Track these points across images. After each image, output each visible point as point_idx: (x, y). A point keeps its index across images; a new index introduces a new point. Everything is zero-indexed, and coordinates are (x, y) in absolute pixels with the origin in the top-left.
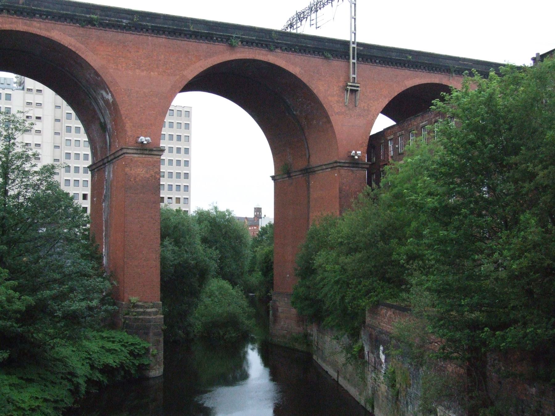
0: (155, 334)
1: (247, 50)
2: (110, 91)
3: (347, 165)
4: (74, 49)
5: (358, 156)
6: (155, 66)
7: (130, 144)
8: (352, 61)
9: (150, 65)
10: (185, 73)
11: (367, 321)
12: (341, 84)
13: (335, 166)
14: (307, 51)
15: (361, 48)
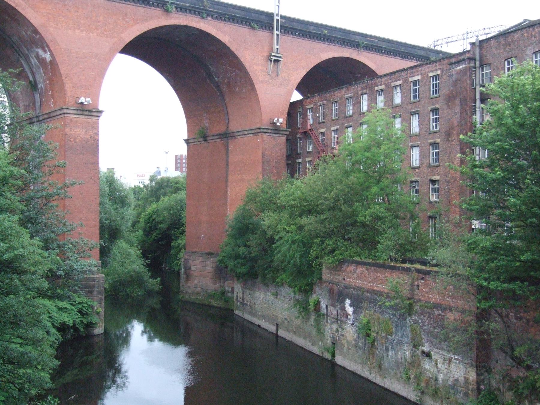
0: (99, 293)
1: (181, 16)
2: (50, 50)
3: (269, 131)
4: (13, 5)
5: (280, 123)
6: (94, 27)
7: (69, 104)
8: (276, 32)
9: (89, 26)
10: (123, 35)
11: (323, 277)
12: (266, 54)
13: (258, 132)
14: (236, 21)
15: (283, 21)
